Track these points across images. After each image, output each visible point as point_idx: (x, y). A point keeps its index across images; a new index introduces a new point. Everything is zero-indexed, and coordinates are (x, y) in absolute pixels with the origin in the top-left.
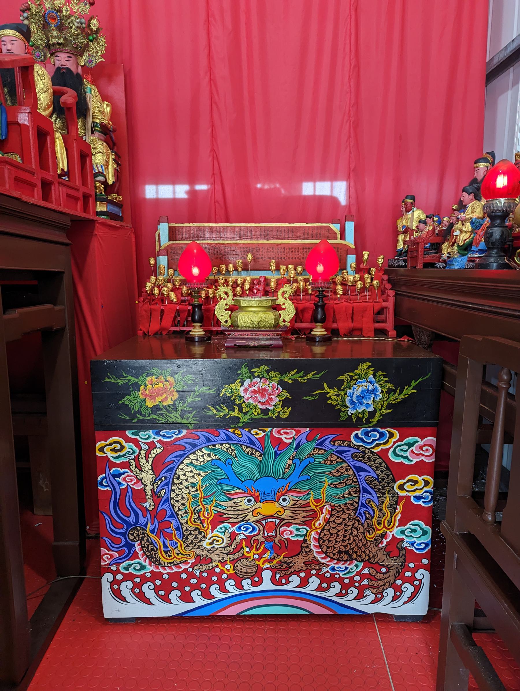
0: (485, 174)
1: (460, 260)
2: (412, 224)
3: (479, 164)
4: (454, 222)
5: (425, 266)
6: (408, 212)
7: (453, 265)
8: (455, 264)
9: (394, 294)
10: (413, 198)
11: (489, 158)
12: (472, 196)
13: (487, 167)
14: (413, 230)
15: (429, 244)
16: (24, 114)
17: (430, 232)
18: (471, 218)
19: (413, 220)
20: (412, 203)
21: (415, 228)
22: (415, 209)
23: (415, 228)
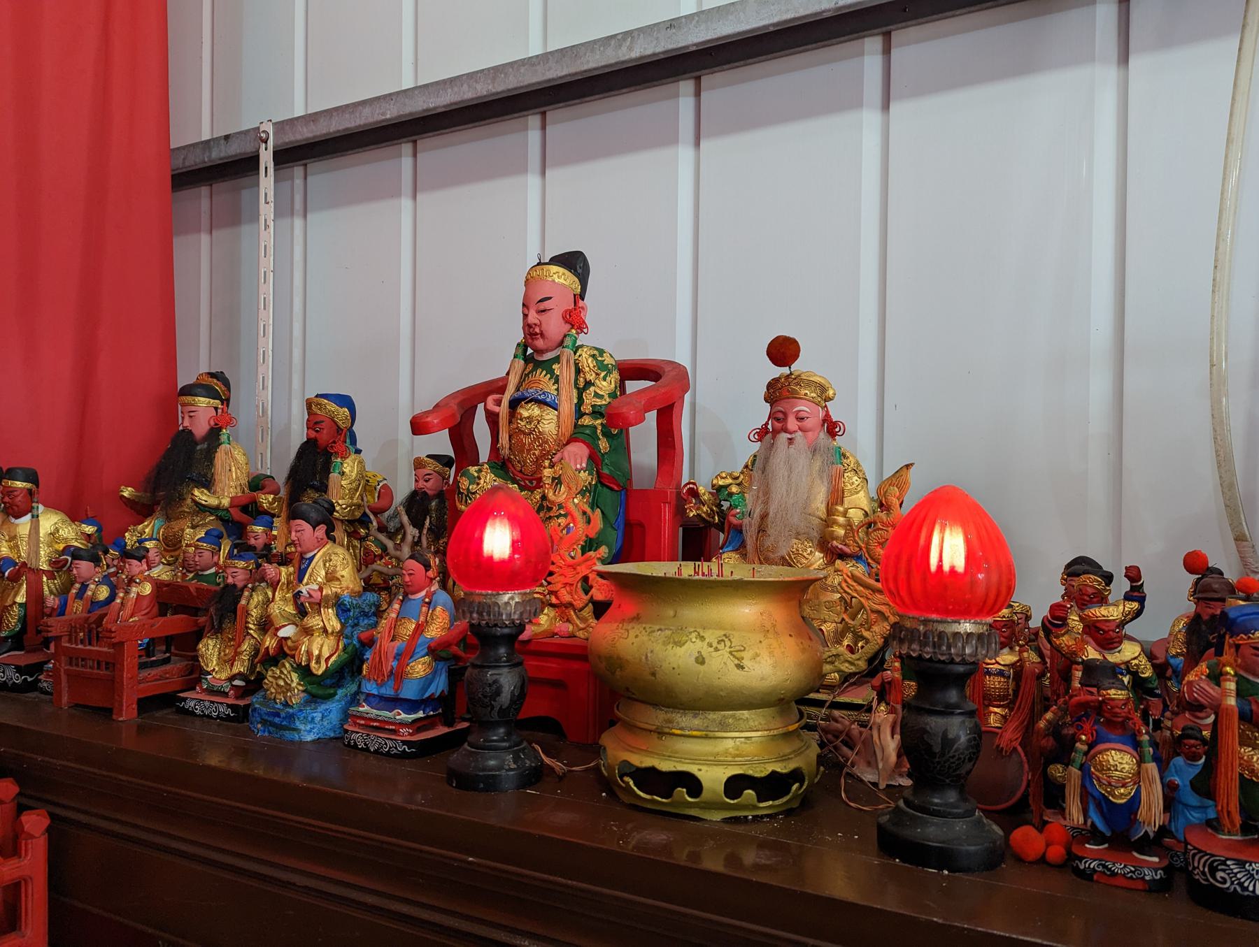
0: (212, 423)
1: (318, 716)
2: (37, 553)
3: (197, 399)
4: (240, 585)
5: (146, 704)
6: (17, 517)
7: (295, 730)
8: (302, 727)
9: (46, 822)
10: (32, 477)
11: (219, 387)
12: (321, 530)
13: (216, 409)
14: (39, 572)
15: (146, 641)
16: (746, 612)
17: (145, 603)
18: (337, 596)
19: (38, 541)
20: (30, 492)
21: (45, 567)
22: (41, 508)
23: (45, 567)
